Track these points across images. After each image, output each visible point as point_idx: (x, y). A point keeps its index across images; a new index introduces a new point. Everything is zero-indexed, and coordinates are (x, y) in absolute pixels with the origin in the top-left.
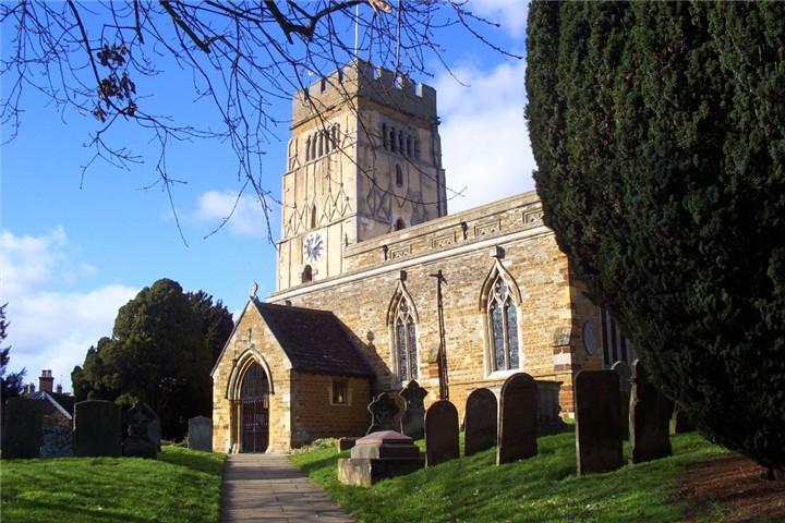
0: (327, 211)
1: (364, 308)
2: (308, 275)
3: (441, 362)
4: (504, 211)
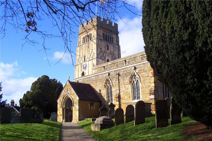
0: (88, 57)
1: (98, 83)
2: (83, 74)
3: (119, 98)
4: (136, 57)
